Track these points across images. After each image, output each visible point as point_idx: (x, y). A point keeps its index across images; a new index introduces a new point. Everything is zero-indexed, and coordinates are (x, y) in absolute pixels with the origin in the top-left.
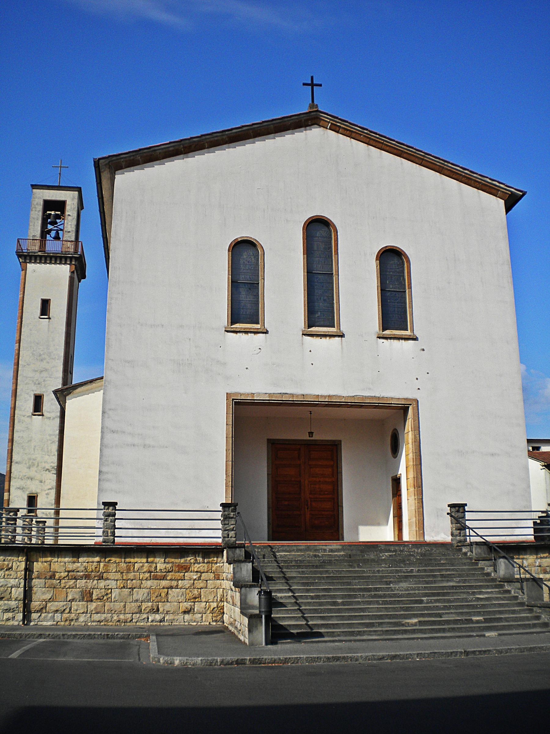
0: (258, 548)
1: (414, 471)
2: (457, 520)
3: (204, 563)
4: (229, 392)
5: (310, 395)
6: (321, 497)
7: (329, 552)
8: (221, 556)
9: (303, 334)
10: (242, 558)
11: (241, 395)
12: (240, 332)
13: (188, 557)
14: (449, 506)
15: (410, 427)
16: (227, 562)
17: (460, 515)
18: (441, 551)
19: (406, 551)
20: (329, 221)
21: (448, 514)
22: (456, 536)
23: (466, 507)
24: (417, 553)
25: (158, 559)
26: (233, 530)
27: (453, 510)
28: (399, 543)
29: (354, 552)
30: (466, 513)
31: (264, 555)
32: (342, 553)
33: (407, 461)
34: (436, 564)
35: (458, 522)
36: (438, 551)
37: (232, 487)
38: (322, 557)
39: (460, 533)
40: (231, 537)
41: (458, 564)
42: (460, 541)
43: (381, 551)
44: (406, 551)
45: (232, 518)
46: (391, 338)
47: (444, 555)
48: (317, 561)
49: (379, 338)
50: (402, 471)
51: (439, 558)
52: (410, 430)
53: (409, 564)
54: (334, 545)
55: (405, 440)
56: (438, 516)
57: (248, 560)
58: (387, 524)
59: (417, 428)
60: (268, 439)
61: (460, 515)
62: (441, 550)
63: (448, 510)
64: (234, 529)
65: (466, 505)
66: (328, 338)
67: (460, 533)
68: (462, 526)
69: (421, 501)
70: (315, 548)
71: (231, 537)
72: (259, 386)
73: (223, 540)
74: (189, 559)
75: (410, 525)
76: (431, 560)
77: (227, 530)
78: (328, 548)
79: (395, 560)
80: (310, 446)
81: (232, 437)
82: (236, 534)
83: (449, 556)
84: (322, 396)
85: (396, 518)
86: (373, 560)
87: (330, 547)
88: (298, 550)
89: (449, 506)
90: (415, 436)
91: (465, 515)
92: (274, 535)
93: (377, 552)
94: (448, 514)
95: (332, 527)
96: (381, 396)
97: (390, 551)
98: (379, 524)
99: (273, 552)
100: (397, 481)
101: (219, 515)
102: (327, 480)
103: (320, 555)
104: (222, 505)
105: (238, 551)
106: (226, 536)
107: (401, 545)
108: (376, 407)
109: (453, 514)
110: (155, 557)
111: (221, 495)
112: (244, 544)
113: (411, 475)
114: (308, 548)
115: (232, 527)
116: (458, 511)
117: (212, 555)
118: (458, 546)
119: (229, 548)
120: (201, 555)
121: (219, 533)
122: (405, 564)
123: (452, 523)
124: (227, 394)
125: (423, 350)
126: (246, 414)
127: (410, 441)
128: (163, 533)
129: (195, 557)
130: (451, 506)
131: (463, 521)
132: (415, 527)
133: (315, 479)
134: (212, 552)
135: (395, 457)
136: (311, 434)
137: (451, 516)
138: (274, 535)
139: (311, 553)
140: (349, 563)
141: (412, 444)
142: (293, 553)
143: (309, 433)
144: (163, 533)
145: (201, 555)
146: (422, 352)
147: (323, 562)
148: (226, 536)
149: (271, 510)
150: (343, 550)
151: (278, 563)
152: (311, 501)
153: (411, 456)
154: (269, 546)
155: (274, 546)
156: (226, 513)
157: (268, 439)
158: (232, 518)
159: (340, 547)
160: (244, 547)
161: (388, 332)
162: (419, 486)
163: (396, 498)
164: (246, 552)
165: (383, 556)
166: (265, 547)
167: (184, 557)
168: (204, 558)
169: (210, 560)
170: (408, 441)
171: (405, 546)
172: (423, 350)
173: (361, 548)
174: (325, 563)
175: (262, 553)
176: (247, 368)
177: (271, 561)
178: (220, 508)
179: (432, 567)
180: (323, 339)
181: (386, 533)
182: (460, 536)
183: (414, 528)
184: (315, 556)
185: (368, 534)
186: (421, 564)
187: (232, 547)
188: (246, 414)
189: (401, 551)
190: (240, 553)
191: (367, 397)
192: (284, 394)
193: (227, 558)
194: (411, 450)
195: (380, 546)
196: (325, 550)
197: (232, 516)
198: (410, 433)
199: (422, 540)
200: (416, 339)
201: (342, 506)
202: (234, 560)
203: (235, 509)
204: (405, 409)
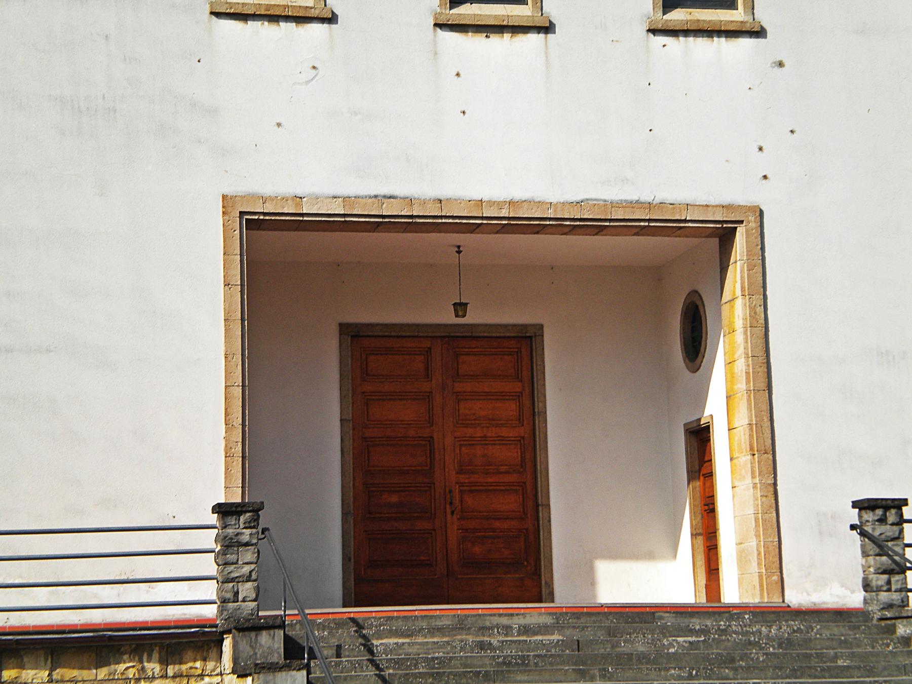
0: (322, 627)
1: (750, 409)
2: (879, 546)
3: (165, 676)
4: (229, 191)
5: (458, 201)
6: (490, 480)
7: (519, 635)
8: (213, 653)
9: (436, 25)
10: (278, 656)
11: (265, 200)
12: (254, 17)
13: (118, 663)
14: (855, 504)
15: (738, 286)
16: (233, 672)
17: (889, 530)
18: (836, 631)
19: (735, 632)
20: (700, 355)
21: (853, 527)
22: (879, 589)
23: (904, 508)
24: (768, 637)
25: (34, 672)
26: (249, 579)
27: (869, 516)
28: (713, 608)
29: (589, 634)
30: (905, 525)
31: (339, 647)
32: (556, 637)
33: (730, 378)
34: (823, 670)
35: (882, 551)
36: (826, 633)
37: (243, 457)
38: (501, 648)
39: (889, 582)
40: (244, 601)
41: (885, 669)
42: (889, 606)
43: (665, 631)
44: (735, 632)
45: (247, 544)
46: (686, 33)
47: (845, 643)
48: (487, 661)
49: (653, 31)
50: (715, 409)
51: (832, 652)
52: (738, 292)
53: (748, 668)
54: (531, 614)
55: (725, 321)
56: (821, 533)
57: (296, 663)
58: (675, 556)
59: (759, 289)
60: (341, 325)
61: (889, 530)
62: (838, 630)
63: (853, 516)
64: (254, 576)
65: (905, 502)
66: (507, 36)
67: (889, 582)
68: (894, 561)
69: (772, 491)
70: (480, 623)
71: (244, 601)
72: (318, 175)
73: (221, 610)
74: (122, 667)
75: (742, 560)
76: (808, 657)
77: (232, 580)
78: (516, 622)
79: (706, 658)
80: (457, 341)
81: (242, 319)
82: (258, 590)
83: (859, 646)
84: (491, 203)
85: (700, 540)
86: (643, 658)
87: (522, 621)
88: (433, 631)
89: (855, 504)
90: (753, 309)
91: (901, 531)
92: (364, 586)
93: (652, 632)
94: (853, 527)
95: (515, 560)
96: (657, 201)
97: (691, 632)
98: (650, 556)
99: (364, 637)
100: (700, 436)
101: (208, 539)
102: (506, 432)
103: (495, 642)
104: (222, 510)
105: (264, 638)
106: (229, 595)
107: (720, 614)
108: (641, 231)
109: (868, 528)
110: (22, 667)
111: (210, 478)
112: (282, 618)
113: (742, 418)
114: (460, 625)
115: (246, 569)
116: (882, 520)
117: (189, 654)
118: (881, 619)
119: (241, 629)
120: (156, 655)
121: (209, 590)
122: (735, 669)
123: (865, 554)
124: (224, 197)
125: (781, 64)
126: (280, 253)
127: (739, 324)
128: (41, 597)
129: (141, 661)
130: (863, 505)
131: (898, 549)
132: (754, 564)
133: (470, 431)
134: (189, 645)
135: (695, 370)
136: (460, 308)
137: (863, 534)
138: (364, 586)
139: (470, 638)
140: (576, 664)
141: (745, 333)
142: (420, 640)
143: (454, 305)
144: (41, 597)
145: (156, 655)
146: (778, 70)
147: (504, 663)
148: (229, 595)
149: (351, 519)
150: (557, 627)
151: (377, 667)
152: (461, 491)
153: (740, 365)
154: (353, 620)
155: (365, 619)
156: (230, 531)
157: (341, 325)
158: (247, 544)
159: (549, 620)
160: (282, 626)
161: (678, 16)
162: (765, 449)
163: (698, 484)
164: (288, 640)
165: (671, 645)
166: (340, 624)
167: (107, 664)
168: (165, 662)
169: (184, 667)
170: (731, 323)
171: (731, 617)
172: (781, 64)
173: (607, 624)
174: (510, 663)
175: (335, 642)
176: (279, 125)
177: (360, 663)
178: (213, 519)
179: (810, 676)
180: (495, 39)
181: (669, 580)
182: (889, 590)
183: (754, 567)
184: (482, 646)
185: (621, 583)
186: (780, 668)
187: (248, 627)
188: (280, 253)
189: (723, 632)
190: (271, 644)
191: (614, 205)
192: (385, 197)
193: (235, 660)
194: (741, 351)
195: (661, 618)
196: (507, 629)
197: (245, 538)
198: (739, 303)
199: (776, 600)
200: (759, 33)
201: (548, 506)
202: (256, 665)
203: (256, 519)
204: (725, 235)
